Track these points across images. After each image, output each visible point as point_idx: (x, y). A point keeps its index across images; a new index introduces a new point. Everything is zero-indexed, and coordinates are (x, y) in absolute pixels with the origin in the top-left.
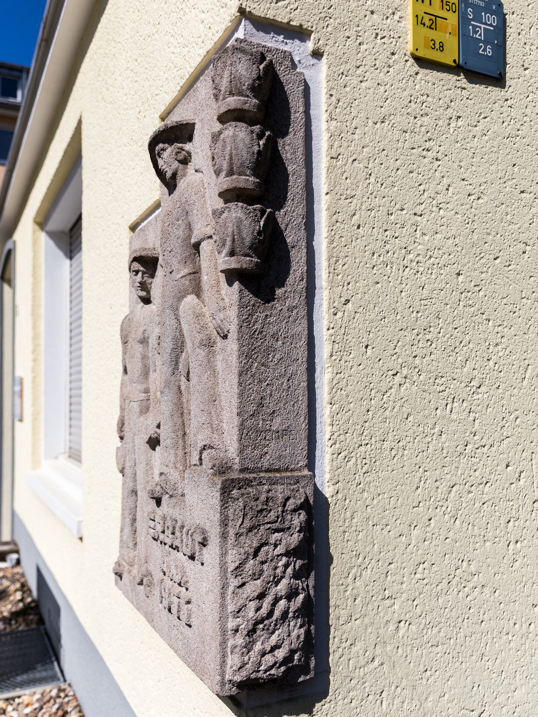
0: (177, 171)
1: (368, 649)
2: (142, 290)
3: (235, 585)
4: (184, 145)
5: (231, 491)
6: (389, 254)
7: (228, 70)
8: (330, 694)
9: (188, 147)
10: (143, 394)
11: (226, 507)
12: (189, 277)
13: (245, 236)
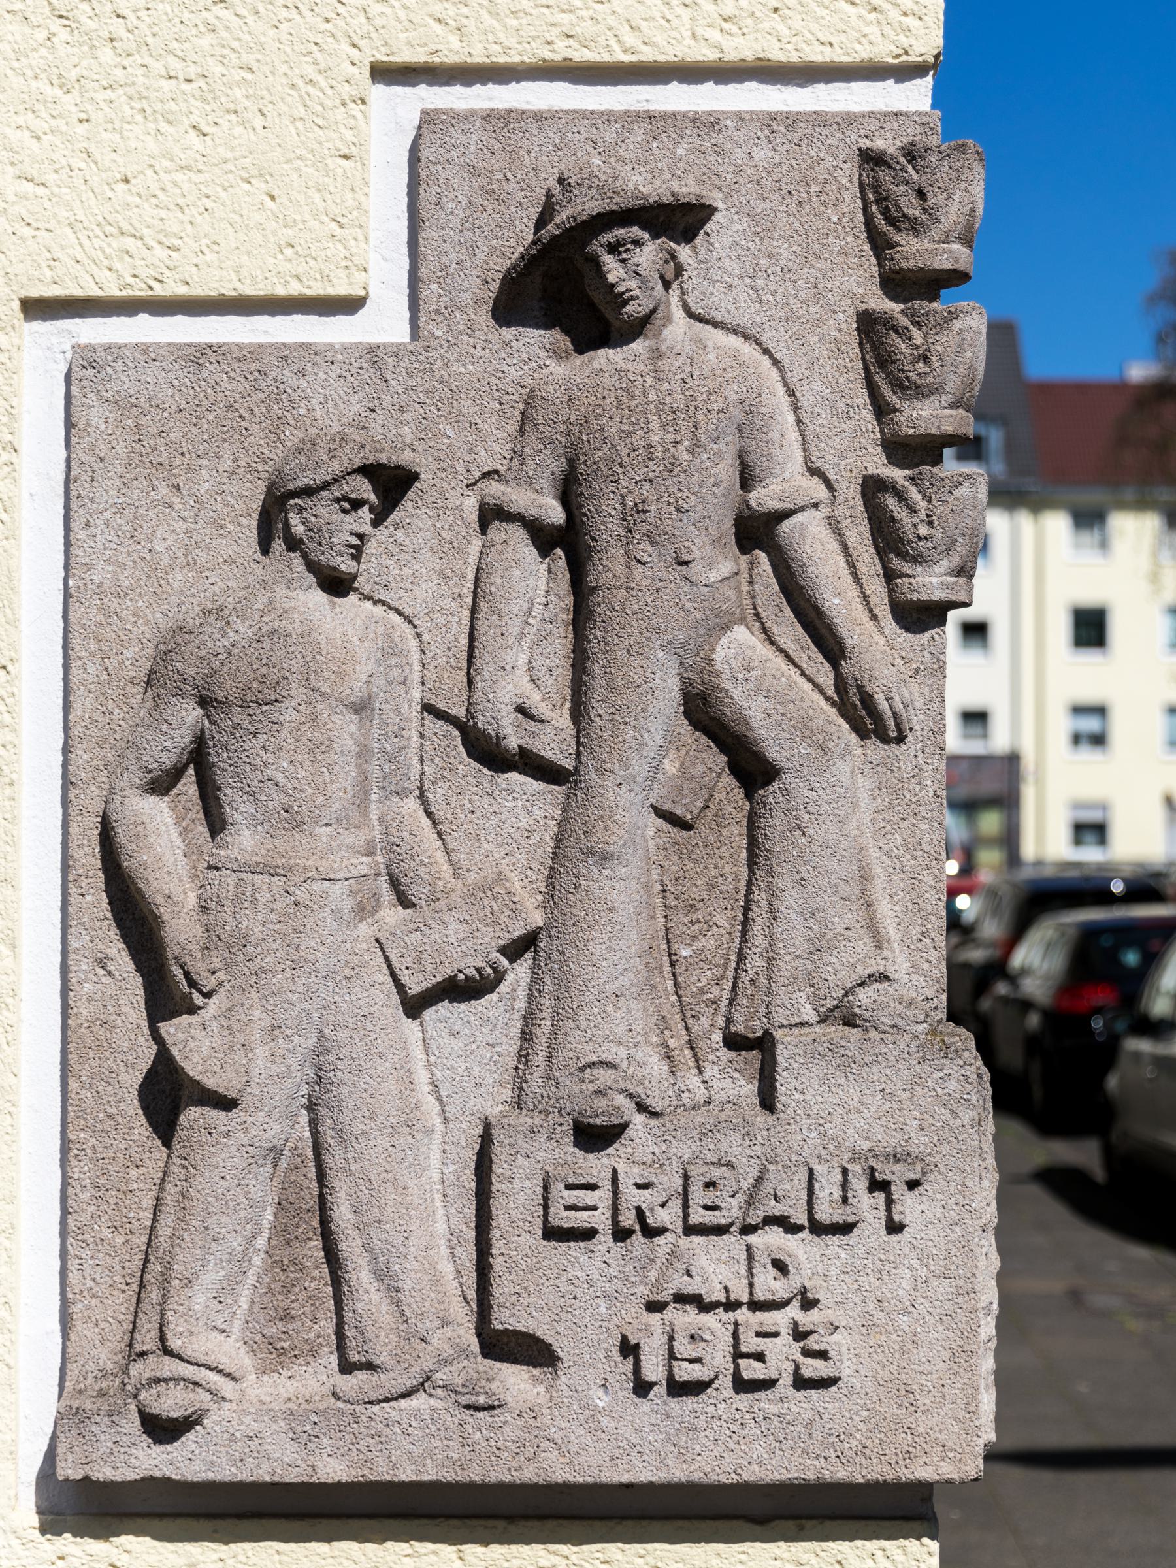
9: (684, 252)
10: (365, 859)
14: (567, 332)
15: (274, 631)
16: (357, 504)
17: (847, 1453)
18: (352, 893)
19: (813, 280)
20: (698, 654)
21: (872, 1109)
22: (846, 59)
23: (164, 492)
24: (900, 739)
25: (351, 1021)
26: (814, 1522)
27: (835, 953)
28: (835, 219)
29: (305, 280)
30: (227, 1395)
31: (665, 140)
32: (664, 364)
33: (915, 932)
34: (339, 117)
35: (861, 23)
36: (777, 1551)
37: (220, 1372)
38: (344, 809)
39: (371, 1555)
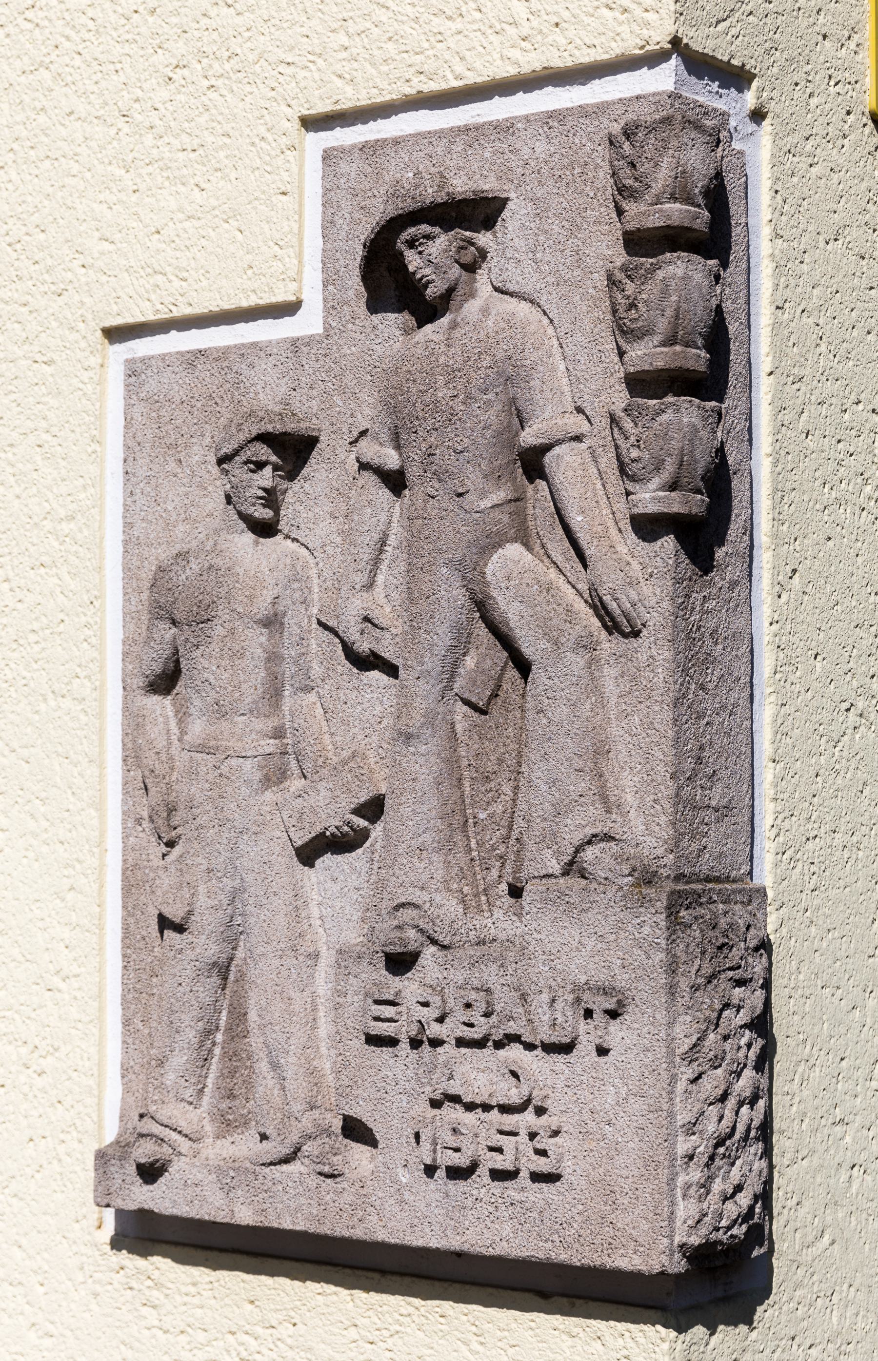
0: (456, 284)
1: (818, 1213)
2: (264, 506)
3: (688, 1076)
4: (475, 235)
5: (678, 912)
6: (843, 485)
7: (673, 157)
8: (774, 1291)
9: (483, 239)
10: (272, 741)
11: (674, 940)
12: (507, 508)
13: (698, 456)
14: (412, 313)
15: (211, 567)
16: (260, 465)
17: (567, 1238)
18: (261, 767)
19: (575, 248)
20: (475, 569)
21: (589, 949)
22: (606, 57)
23: (172, 466)
24: (636, 634)
25: (256, 866)
26: (581, 1301)
27: (570, 816)
28: (592, 195)
29: (258, 292)
30: (183, 1151)
31: (477, 146)
32: (457, 333)
33: (649, 799)
34: (280, 163)
35: (615, 24)
36: (556, 1323)
37: (180, 1132)
38: (253, 702)
39: (297, 1291)
